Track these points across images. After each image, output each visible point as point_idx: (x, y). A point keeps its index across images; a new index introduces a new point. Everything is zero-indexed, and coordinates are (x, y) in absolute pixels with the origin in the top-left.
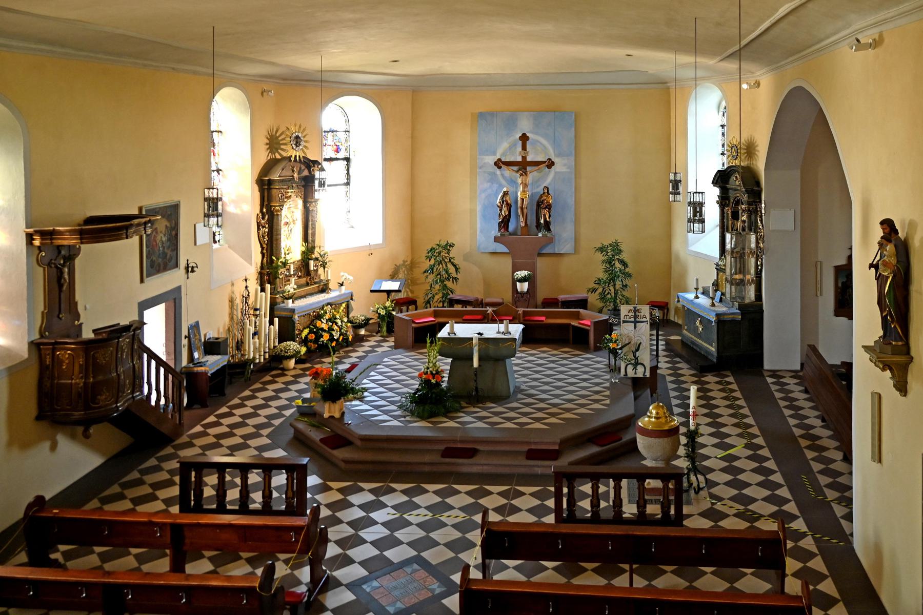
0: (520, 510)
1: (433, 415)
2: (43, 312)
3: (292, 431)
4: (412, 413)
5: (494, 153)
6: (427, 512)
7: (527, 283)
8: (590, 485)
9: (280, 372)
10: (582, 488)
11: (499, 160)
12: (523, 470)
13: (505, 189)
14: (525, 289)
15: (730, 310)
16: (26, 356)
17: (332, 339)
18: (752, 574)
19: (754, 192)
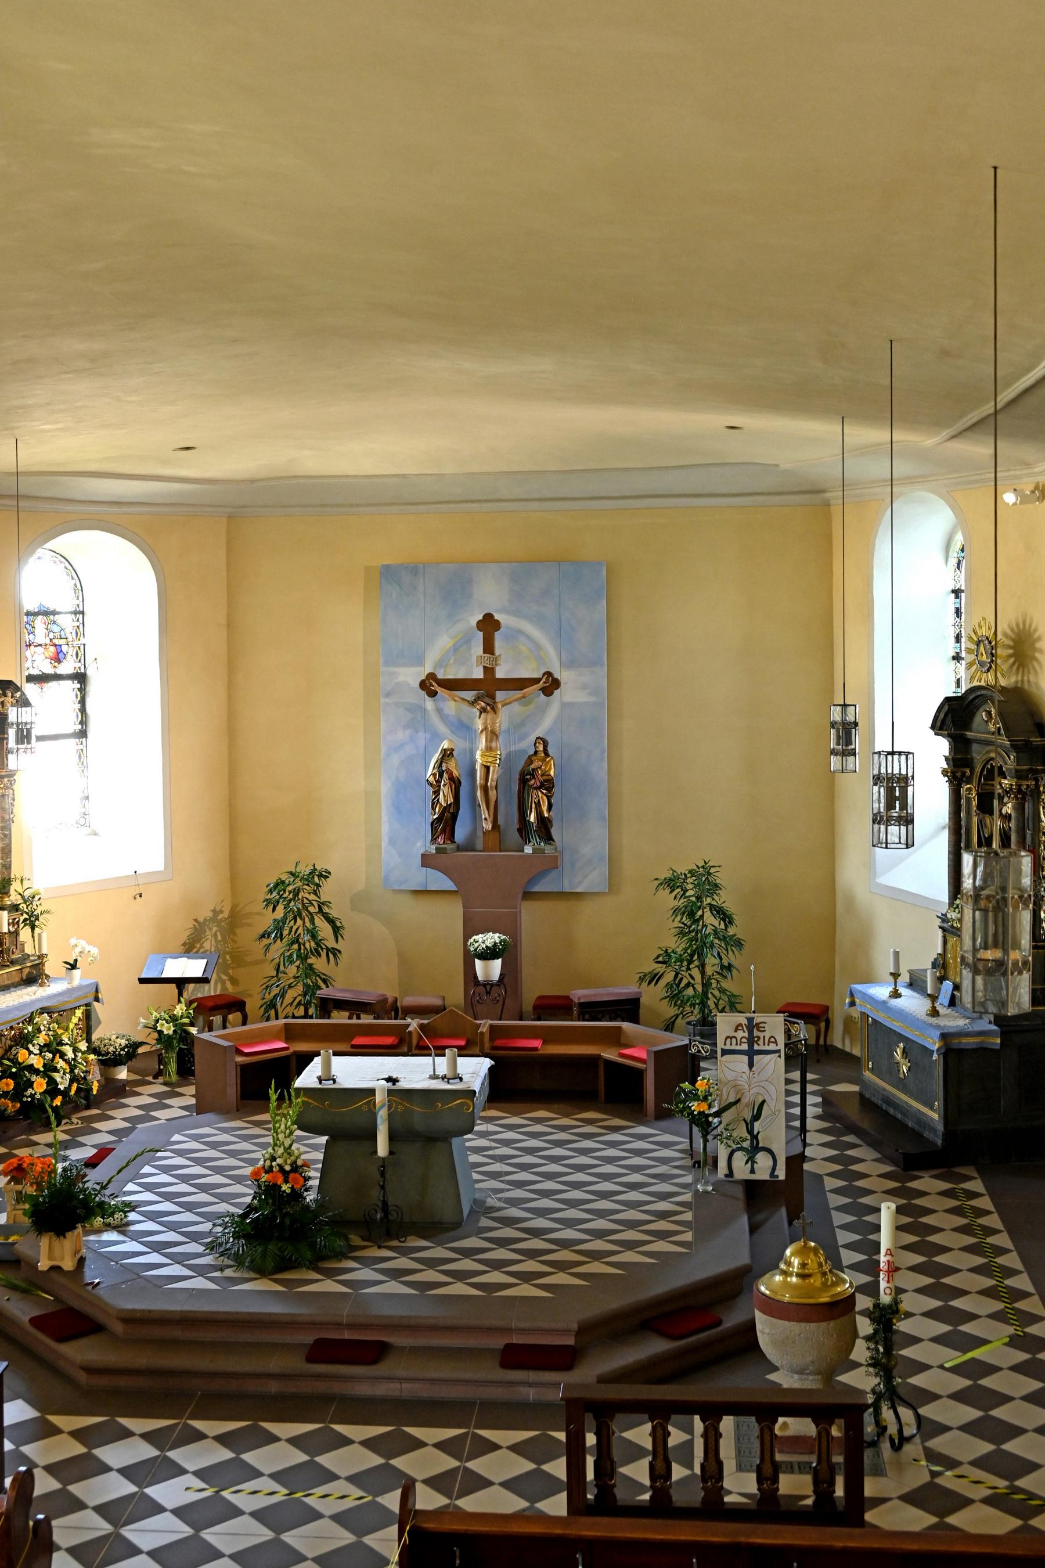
1: (285, 1265)
5: (420, 661)
7: (498, 963)
8: (648, 1427)
11: (432, 676)
13: (445, 745)
17: (53, 1089)
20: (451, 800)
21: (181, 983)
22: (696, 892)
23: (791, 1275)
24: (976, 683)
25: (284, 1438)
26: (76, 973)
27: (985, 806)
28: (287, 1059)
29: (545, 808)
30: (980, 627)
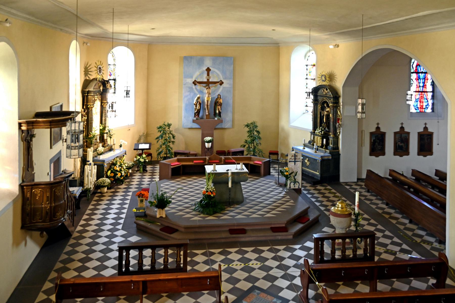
0: (202, 263)
1: (215, 212)
2: (23, 168)
3: (135, 225)
4: (202, 213)
6: (240, 263)
8: (163, 250)
9: (100, 194)
10: (160, 252)
11: (195, 81)
13: (198, 96)
14: (210, 146)
15: (326, 154)
16: (18, 193)
17: (121, 176)
18: (207, 293)
19: (336, 97)
22: (252, 128)
26: (122, 148)
27: (323, 109)
28: (180, 166)
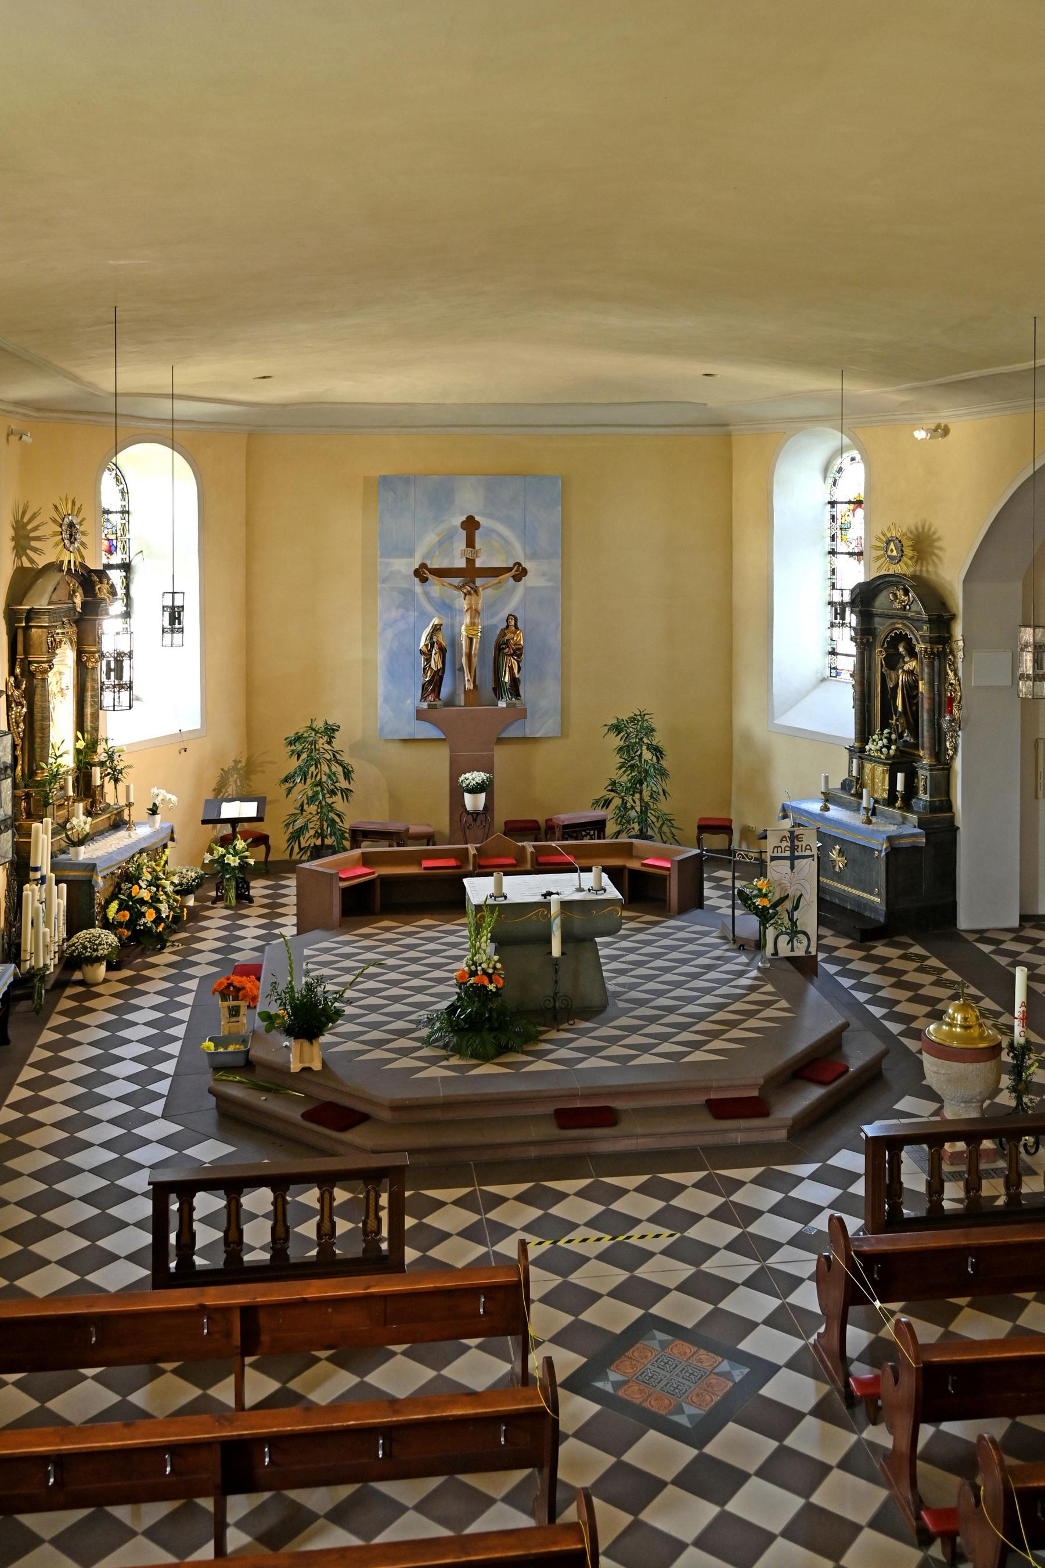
1: (503, 1049)
5: (410, 553)
7: (483, 795)
9: (81, 989)
11: (423, 566)
12: (709, 1140)
13: (436, 621)
17: (158, 920)
19: (941, 621)
20: (440, 666)
21: (234, 822)
22: (633, 734)
23: (955, 1026)
24: (883, 573)
25: (632, 1193)
26: (158, 817)
28: (373, 881)
29: (516, 671)
30: (889, 530)
